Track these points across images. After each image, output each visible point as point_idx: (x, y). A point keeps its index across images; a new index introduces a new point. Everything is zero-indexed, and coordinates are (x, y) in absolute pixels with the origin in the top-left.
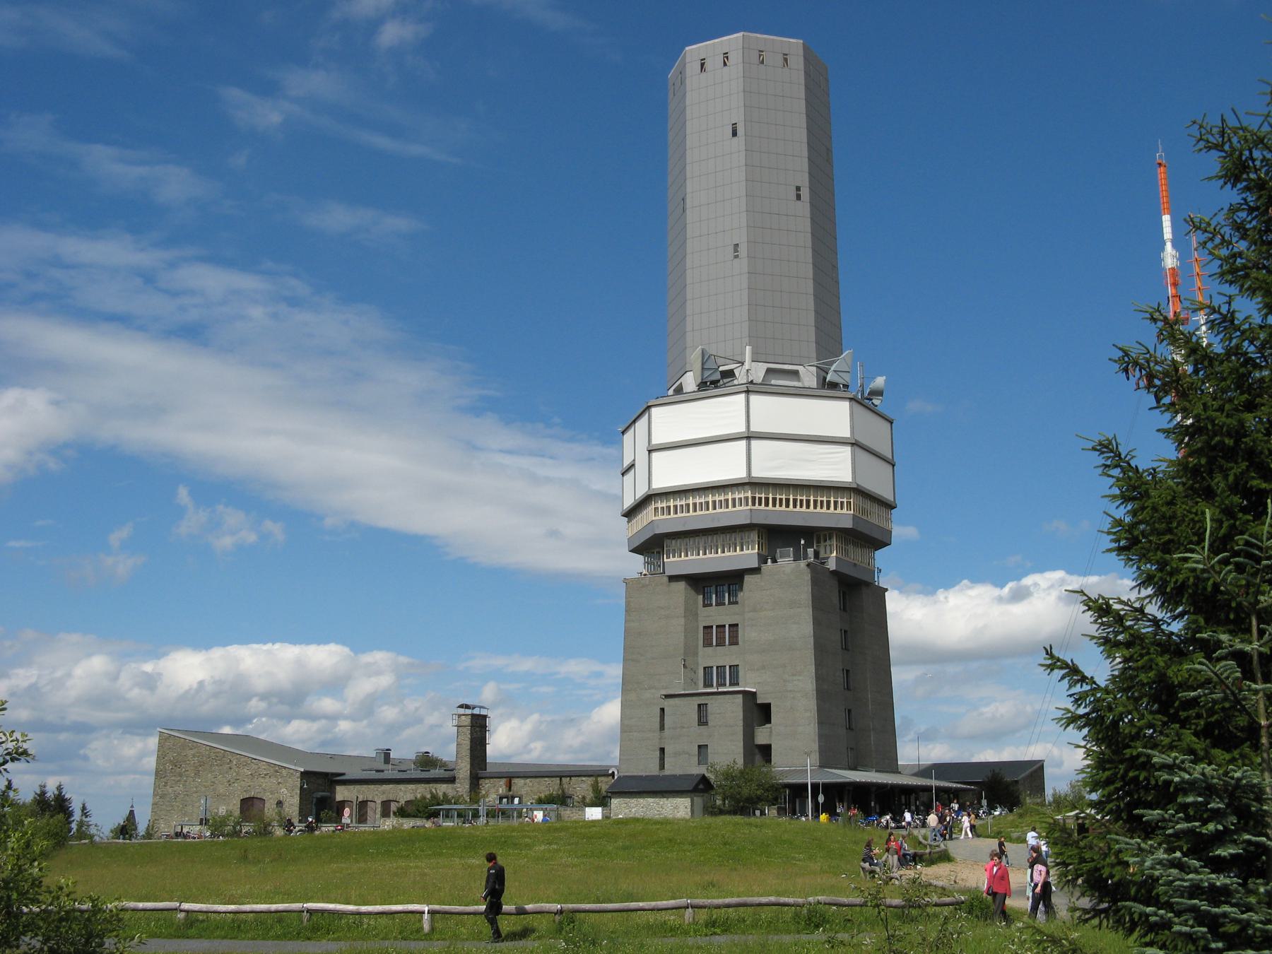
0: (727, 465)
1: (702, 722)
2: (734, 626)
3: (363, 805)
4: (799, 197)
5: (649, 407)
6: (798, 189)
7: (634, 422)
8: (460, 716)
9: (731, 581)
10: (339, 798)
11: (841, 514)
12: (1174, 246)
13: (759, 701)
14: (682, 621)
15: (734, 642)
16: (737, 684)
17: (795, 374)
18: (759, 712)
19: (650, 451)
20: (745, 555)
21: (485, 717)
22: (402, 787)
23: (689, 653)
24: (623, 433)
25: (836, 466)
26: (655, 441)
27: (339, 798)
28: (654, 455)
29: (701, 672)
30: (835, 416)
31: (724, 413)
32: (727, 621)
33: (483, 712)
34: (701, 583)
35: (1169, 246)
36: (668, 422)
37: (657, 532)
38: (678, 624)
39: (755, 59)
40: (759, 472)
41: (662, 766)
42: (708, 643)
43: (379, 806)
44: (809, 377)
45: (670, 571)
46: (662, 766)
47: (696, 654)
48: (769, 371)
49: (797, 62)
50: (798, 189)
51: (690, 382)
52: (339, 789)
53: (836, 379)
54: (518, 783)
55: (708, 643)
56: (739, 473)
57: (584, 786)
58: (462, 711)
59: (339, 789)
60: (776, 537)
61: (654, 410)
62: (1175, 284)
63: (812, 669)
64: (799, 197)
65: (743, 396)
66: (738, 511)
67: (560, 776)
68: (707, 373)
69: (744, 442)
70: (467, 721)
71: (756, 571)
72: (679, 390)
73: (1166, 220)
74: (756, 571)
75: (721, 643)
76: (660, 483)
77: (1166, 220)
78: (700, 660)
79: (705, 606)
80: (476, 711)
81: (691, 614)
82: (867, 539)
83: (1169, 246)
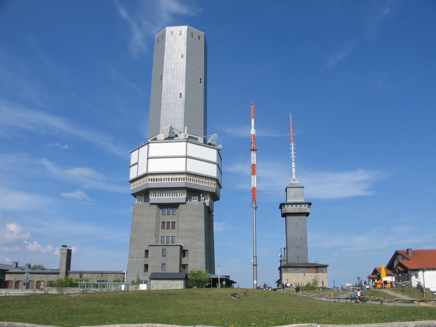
0: (178, 166)
1: (164, 256)
2: (174, 223)
3: (38, 283)
4: (201, 82)
5: (148, 143)
6: (201, 79)
7: (139, 148)
8: (62, 249)
9: (175, 206)
10: (6, 279)
11: (211, 186)
12: (254, 128)
13: (183, 249)
14: (155, 219)
15: (173, 227)
16: (174, 243)
17: (197, 139)
18: (183, 253)
19: (148, 159)
20: (181, 197)
21: (71, 250)
22: (36, 275)
23: (157, 231)
24: (131, 153)
25: (211, 171)
26: (150, 155)
27: (6, 279)
28: (149, 160)
29: (160, 238)
30: (211, 154)
31: (178, 148)
32: (171, 221)
33: (70, 249)
34: (162, 206)
35: (253, 128)
36: (155, 149)
37: (149, 187)
38: (153, 221)
39: (191, 35)
40: (190, 170)
41: (255, 276)
42: (163, 227)
43: (35, 283)
44: (201, 140)
45: (151, 202)
46: (255, 276)
47: (159, 231)
48: (189, 137)
49: (202, 39)
50: (201, 79)
51: (161, 137)
52: (7, 275)
53: (211, 142)
54: (85, 276)
55: (163, 227)
56: (183, 169)
57: (112, 277)
58: (63, 248)
59: (7, 275)
60: (192, 192)
61: (150, 144)
62: (254, 139)
63: (204, 239)
64: (201, 82)
65: (185, 143)
66: (181, 183)
67: (102, 273)
68: (171, 134)
69: (185, 158)
70: (65, 251)
71: (185, 203)
72: (156, 139)
73: (253, 120)
74: (185, 203)
75: (168, 228)
76: (150, 170)
77: (253, 120)
78: (160, 234)
79: (163, 215)
80: (68, 248)
81: (158, 217)
82: (215, 197)
83: (253, 128)
